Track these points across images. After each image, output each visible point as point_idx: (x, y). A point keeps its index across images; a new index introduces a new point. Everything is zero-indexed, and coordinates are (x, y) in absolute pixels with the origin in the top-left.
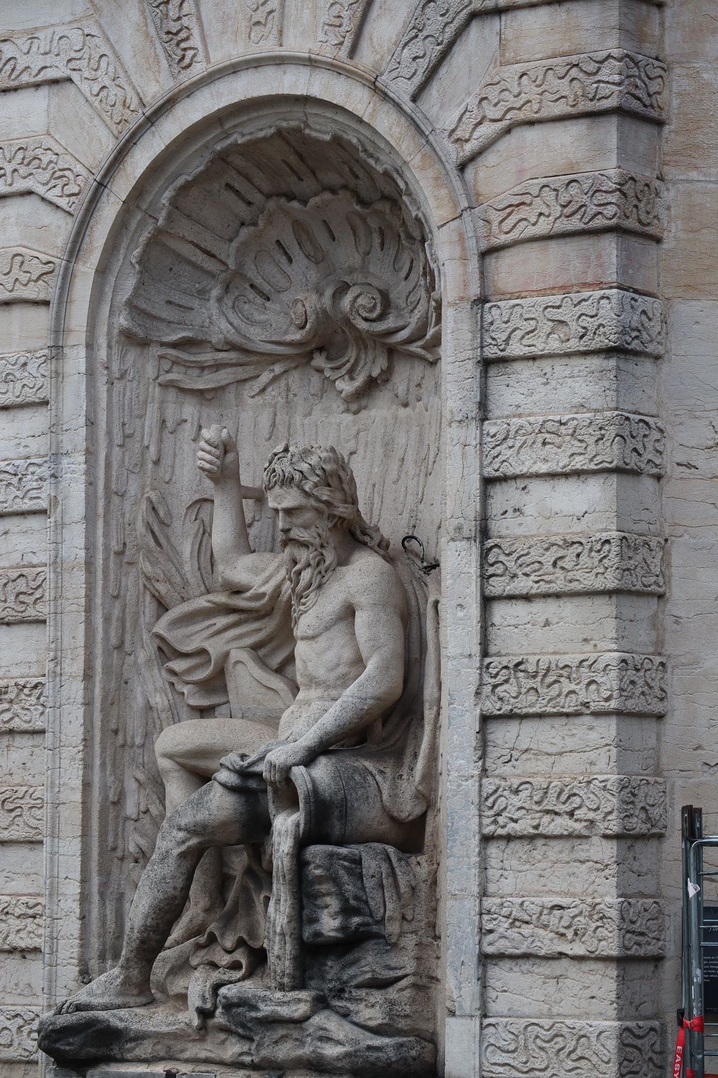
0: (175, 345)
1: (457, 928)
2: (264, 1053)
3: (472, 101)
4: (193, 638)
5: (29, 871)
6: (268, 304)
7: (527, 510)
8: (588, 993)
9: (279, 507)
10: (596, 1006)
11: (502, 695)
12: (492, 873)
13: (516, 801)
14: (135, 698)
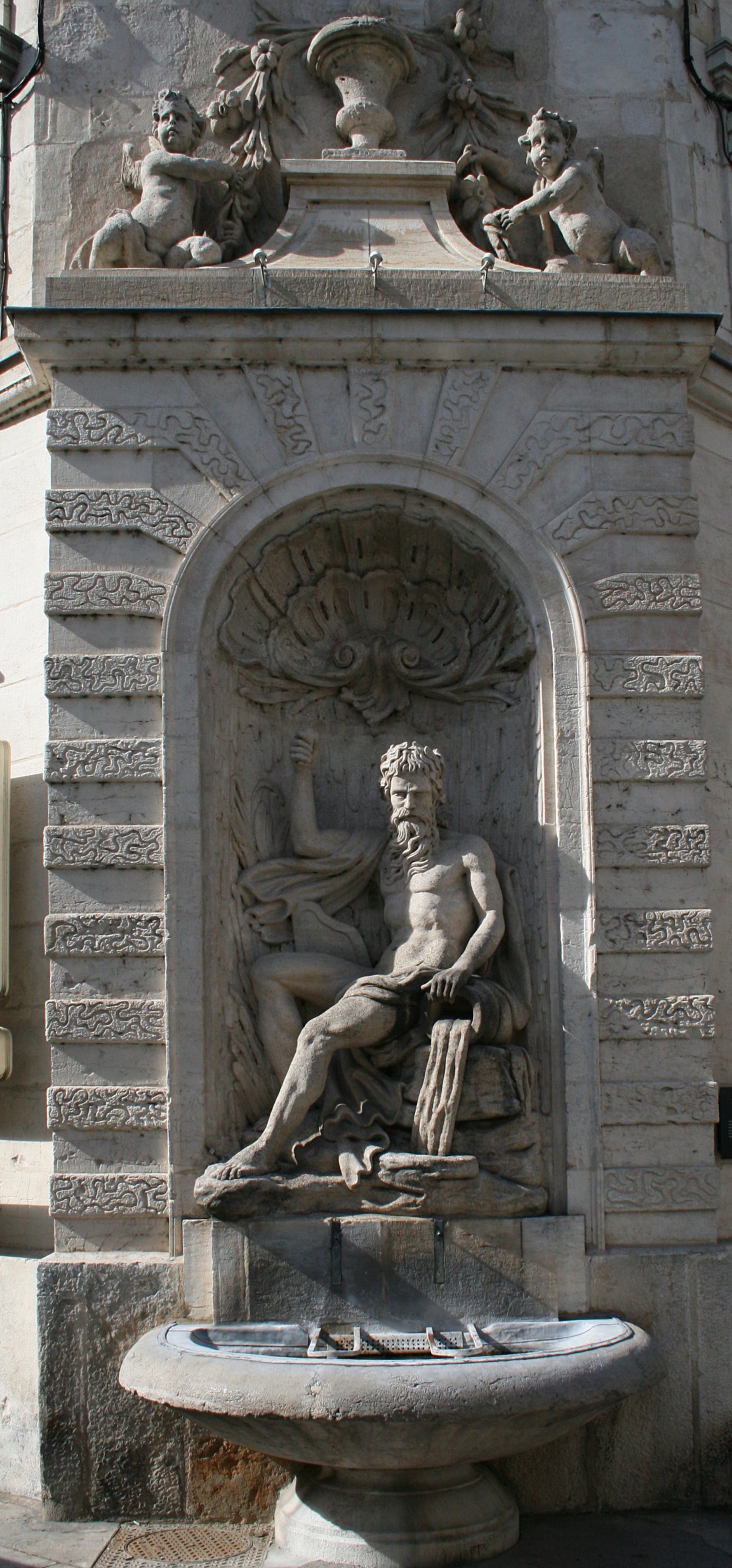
0: (247, 667)
3: (572, 511)
6: (305, 649)
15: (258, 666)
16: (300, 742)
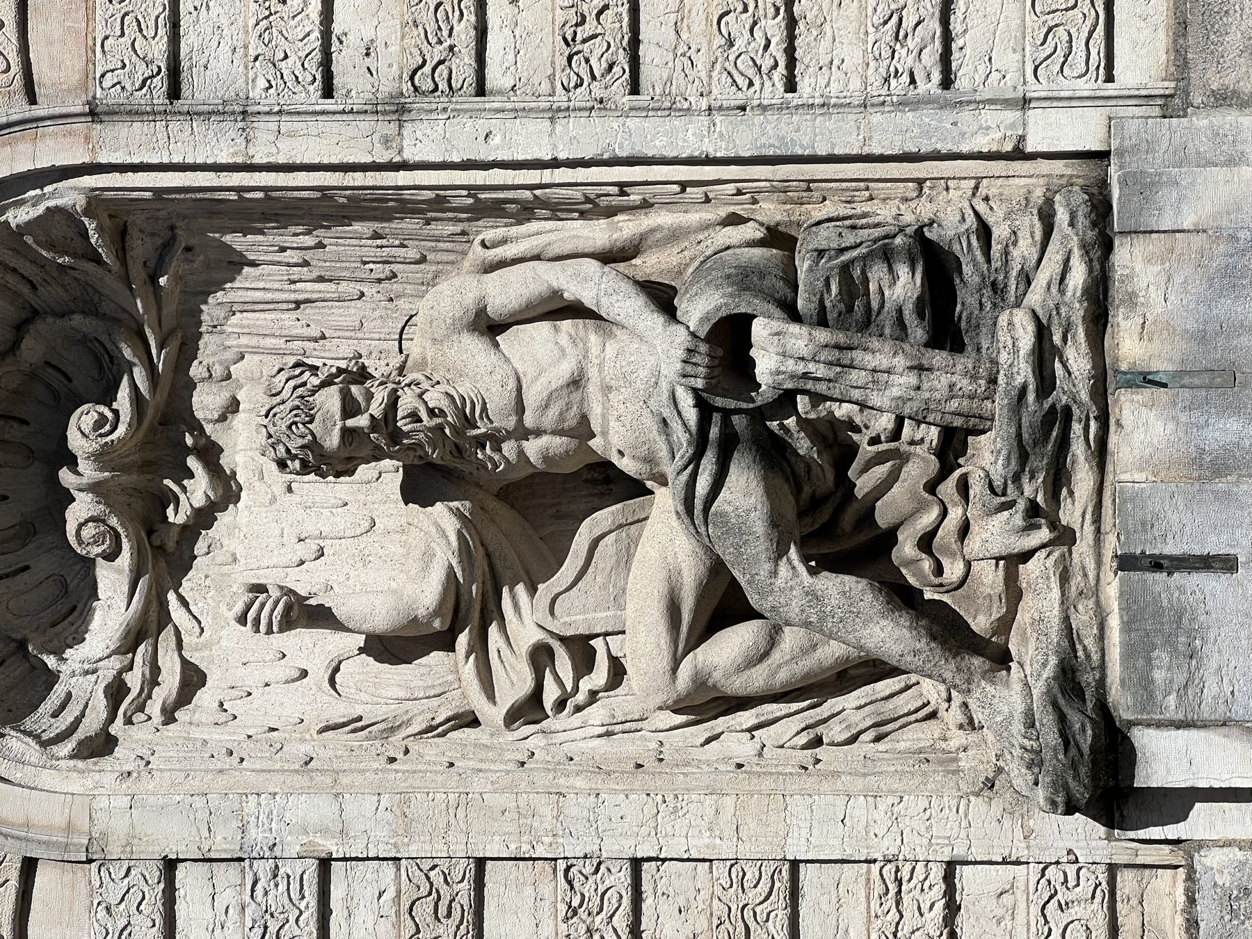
1: (908, 135)
2: (1084, 396)
4: (514, 680)
5: (834, 900)
7: (368, 34)
9: (339, 425)
11: (604, 65)
12: (826, 225)
13: (740, 44)
14: (593, 749)
15: (116, 692)
16: (251, 615)
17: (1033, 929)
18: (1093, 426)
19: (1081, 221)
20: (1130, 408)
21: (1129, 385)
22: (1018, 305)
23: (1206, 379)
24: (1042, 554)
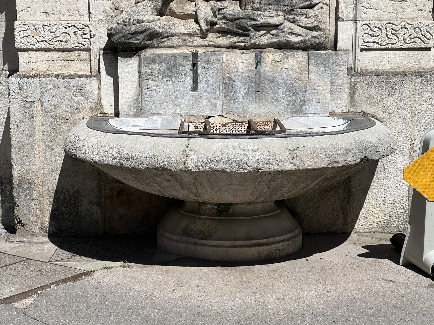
2: (253, 41)
8: (418, 8)
10: (422, 14)
17: (67, 22)
18: (242, 44)
19: (314, 40)
20: (249, 56)
21: (256, 56)
22: (285, 19)
23: (258, 82)
24: (198, 27)
